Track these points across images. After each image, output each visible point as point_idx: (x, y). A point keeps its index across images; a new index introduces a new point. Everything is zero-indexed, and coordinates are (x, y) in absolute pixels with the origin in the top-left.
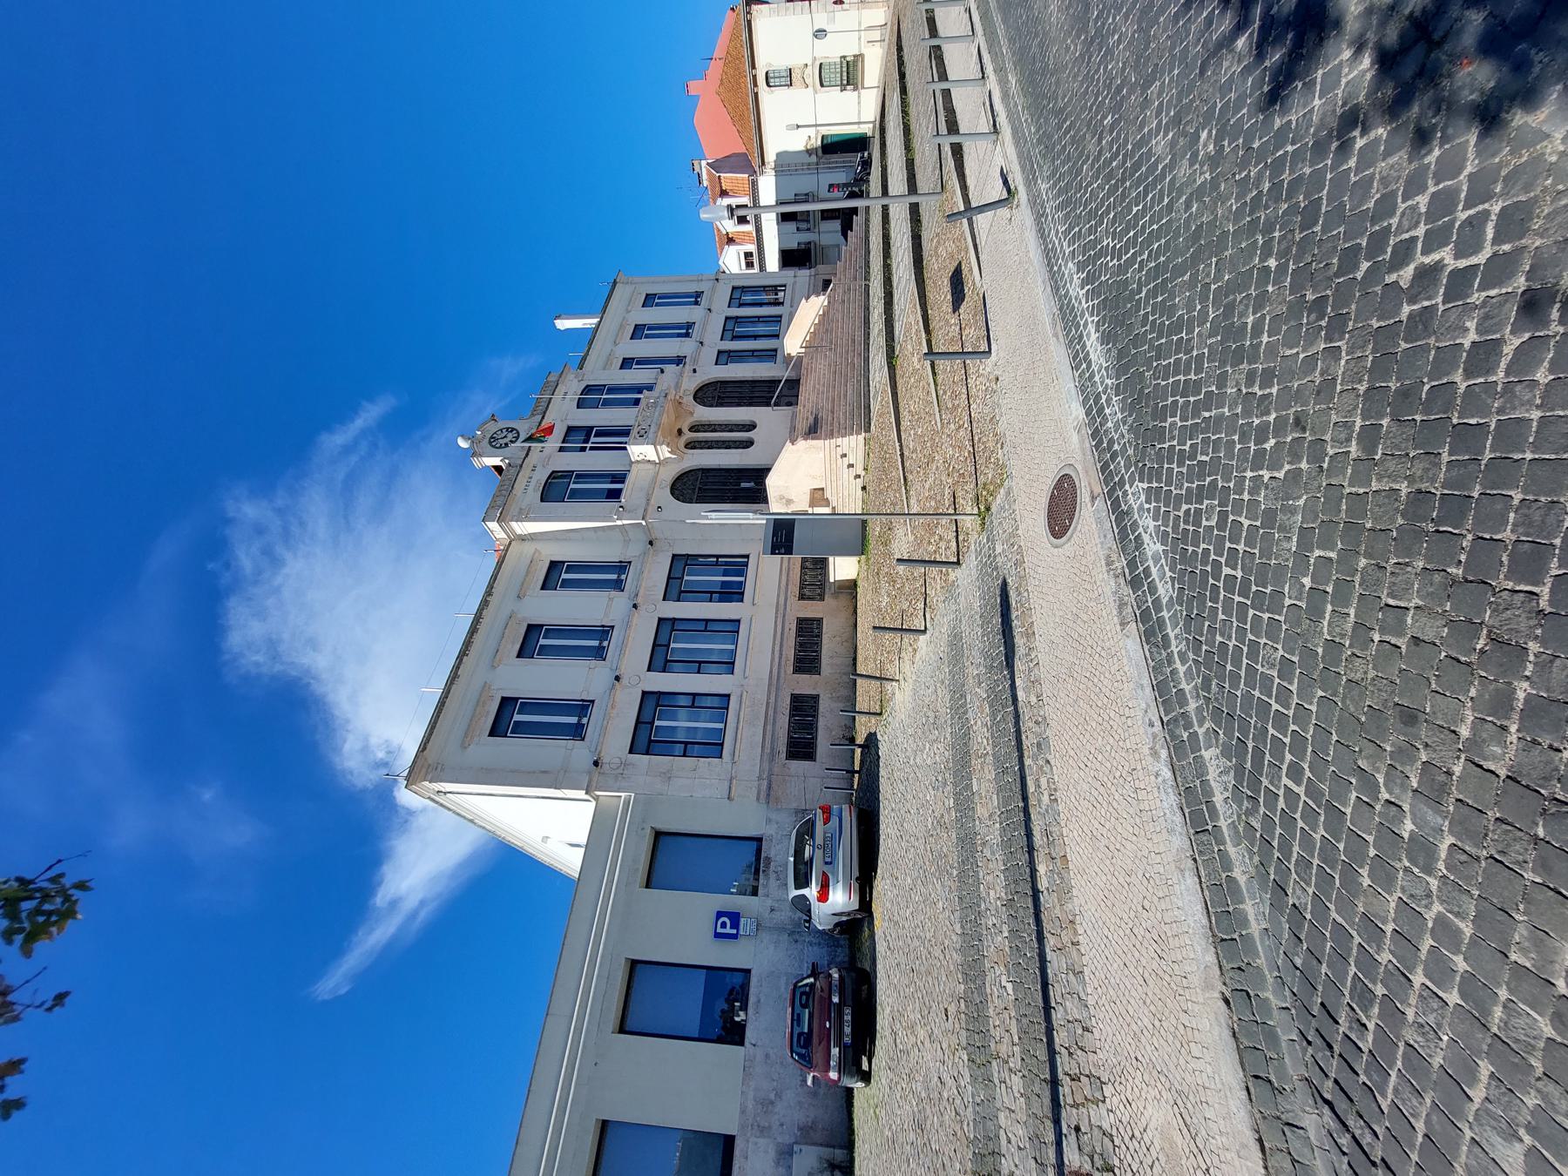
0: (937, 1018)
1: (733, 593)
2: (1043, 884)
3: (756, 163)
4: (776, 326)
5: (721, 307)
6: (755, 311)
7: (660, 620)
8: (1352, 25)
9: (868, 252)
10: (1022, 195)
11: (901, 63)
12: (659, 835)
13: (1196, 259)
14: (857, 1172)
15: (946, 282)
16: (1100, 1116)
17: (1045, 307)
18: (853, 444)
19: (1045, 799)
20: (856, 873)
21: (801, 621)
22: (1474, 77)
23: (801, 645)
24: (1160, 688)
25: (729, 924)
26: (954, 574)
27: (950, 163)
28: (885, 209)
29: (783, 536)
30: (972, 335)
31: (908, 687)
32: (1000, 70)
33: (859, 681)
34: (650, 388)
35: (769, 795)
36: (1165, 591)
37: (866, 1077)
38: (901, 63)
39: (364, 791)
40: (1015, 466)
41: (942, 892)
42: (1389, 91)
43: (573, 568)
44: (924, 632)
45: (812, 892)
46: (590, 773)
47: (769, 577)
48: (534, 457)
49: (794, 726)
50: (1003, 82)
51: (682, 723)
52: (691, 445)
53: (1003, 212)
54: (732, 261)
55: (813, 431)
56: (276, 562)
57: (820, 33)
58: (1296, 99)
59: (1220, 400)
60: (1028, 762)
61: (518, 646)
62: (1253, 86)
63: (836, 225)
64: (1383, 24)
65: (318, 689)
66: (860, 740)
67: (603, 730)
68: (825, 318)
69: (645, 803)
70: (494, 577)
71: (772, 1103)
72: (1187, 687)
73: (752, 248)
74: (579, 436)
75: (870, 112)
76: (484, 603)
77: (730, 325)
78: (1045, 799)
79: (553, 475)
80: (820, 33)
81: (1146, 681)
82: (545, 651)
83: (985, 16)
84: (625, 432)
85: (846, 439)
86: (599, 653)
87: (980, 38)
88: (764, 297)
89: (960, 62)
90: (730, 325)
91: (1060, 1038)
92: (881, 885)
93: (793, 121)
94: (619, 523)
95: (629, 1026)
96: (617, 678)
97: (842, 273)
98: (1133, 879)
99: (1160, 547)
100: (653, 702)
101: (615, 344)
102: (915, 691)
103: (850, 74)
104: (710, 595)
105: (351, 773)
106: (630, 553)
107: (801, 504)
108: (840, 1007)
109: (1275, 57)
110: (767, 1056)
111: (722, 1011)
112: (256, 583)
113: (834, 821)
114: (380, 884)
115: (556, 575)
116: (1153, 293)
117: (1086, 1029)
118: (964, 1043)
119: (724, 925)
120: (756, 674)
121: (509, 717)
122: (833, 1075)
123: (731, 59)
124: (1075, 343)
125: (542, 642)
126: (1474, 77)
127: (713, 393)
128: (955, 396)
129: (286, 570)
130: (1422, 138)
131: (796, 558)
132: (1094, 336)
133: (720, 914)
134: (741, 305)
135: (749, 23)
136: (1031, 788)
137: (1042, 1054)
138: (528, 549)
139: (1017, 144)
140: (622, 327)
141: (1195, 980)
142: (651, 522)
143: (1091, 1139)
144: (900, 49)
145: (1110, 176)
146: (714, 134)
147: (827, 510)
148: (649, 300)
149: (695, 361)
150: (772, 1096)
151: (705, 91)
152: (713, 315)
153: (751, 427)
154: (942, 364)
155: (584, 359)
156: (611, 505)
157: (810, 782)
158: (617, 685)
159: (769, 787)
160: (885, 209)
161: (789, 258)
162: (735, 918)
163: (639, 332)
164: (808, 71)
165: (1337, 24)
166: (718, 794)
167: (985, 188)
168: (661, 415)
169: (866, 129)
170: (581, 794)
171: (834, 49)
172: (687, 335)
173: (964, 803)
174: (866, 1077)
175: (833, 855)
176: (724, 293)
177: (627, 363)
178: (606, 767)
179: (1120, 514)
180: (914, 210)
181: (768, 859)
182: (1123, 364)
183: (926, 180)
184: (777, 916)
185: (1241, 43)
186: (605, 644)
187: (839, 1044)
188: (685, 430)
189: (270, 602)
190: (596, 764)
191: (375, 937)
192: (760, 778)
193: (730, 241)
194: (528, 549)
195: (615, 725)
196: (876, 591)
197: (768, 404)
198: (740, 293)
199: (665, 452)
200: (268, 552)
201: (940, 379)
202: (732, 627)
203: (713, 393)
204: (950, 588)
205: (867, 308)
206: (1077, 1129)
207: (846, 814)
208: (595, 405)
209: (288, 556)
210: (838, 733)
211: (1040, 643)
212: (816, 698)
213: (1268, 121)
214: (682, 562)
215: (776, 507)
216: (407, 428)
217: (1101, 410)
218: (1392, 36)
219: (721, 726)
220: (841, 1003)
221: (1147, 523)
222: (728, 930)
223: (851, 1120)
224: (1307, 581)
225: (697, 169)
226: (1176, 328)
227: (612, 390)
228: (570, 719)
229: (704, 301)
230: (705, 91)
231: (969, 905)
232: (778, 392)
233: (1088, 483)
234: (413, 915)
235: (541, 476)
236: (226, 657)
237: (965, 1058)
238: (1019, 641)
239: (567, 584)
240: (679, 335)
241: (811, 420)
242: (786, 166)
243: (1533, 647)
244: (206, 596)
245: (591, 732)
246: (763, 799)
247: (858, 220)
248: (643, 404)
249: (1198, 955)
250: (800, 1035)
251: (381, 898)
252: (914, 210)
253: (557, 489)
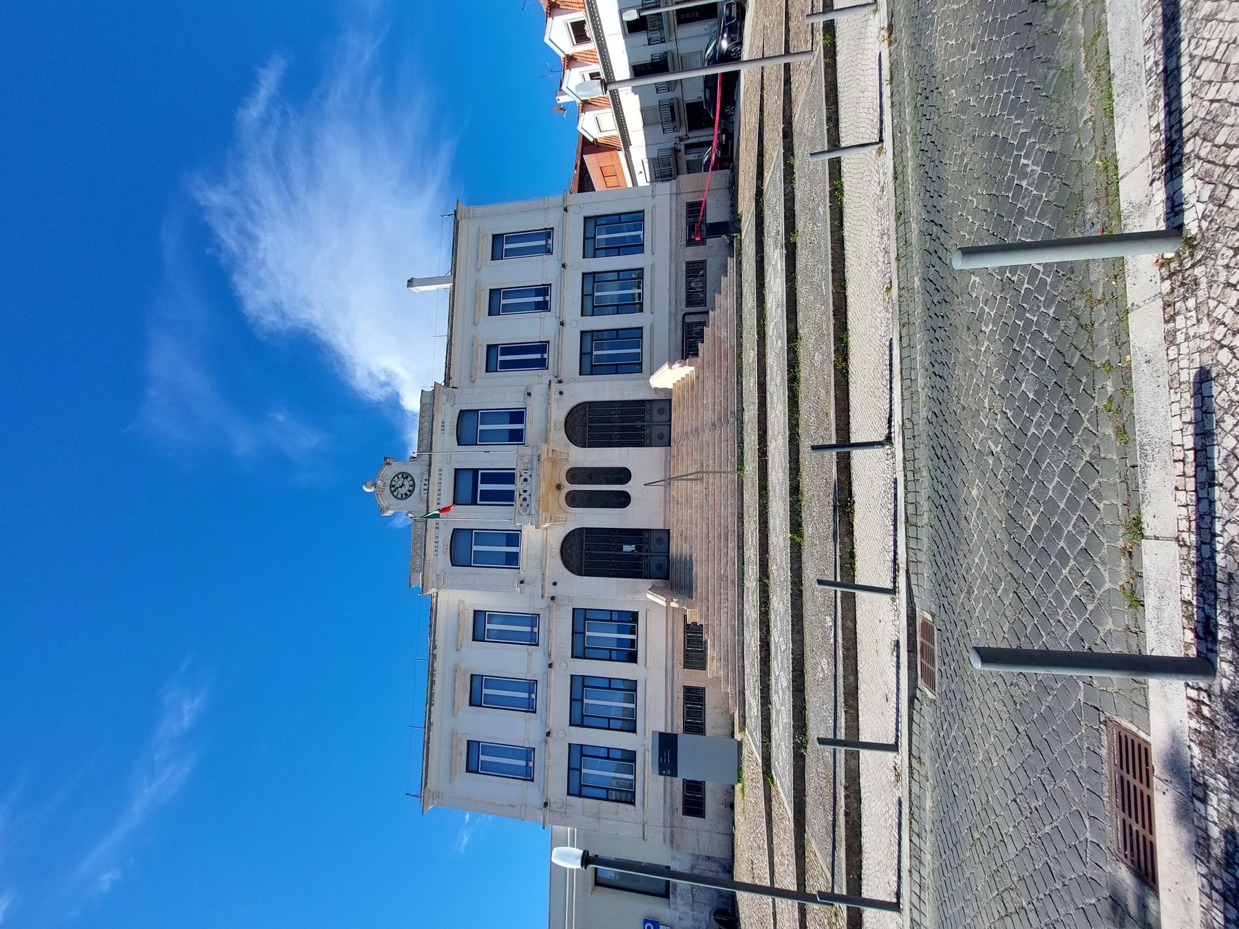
14: (743, 926)
39: (379, 403)
56: (253, 239)
65: (324, 337)
83: (898, 130)
87: (902, 757)
106: (538, 606)
112: (246, 259)
129: (261, 245)
152: (567, 328)
153: (622, 475)
156: (509, 573)
159: (672, 833)
178: (553, 807)
189: (262, 273)
195: (567, 353)
200: (242, 231)
202: (630, 688)
209: (258, 232)
210: (721, 795)
216: (303, 88)
219: (639, 350)
223: (733, 844)
228: (522, 765)
236: (250, 320)
244: (217, 281)
245: (553, 305)
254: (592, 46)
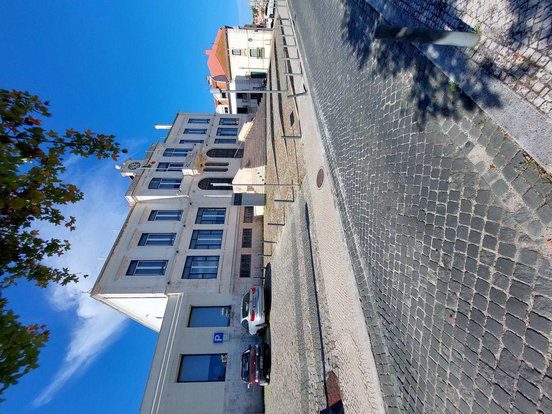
0: (290, 347)
1: (221, 221)
2: (318, 289)
3: (229, 78)
4: (235, 132)
5: (217, 125)
6: (229, 127)
7: (194, 230)
8: (373, 52)
9: (266, 109)
10: (309, 92)
11: (275, 50)
12: (193, 308)
13: (347, 107)
15: (289, 117)
16: (335, 352)
17: (315, 123)
18: (261, 169)
19: (318, 264)
20: (264, 310)
21: (244, 230)
22: (392, 65)
23: (245, 238)
24: (344, 222)
25: (219, 338)
26: (293, 205)
27: (290, 82)
28: (271, 94)
29: (238, 199)
30: (296, 133)
31: (279, 244)
32: (303, 56)
33: (265, 244)
34: (191, 150)
35: (234, 290)
36: (344, 196)
37: (268, 381)
38: (275, 50)
39: (64, 312)
40: (308, 169)
41: (290, 305)
42: (380, 67)
43: (161, 212)
44: (284, 225)
45: (248, 318)
46: (166, 287)
47: (234, 214)
48: (146, 173)
49: (242, 266)
50: (304, 60)
51: (200, 267)
52: (205, 170)
53: (304, 96)
54: (220, 110)
55: (248, 165)
57: (250, 40)
58: (364, 68)
59: (351, 143)
60: (313, 255)
61: (138, 242)
62: (356, 64)
63: (256, 101)
64: (378, 52)
66: (265, 266)
67: (179, 241)
68: (252, 129)
69: (188, 296)
70: (129, 216)
71: (235, 400)
72: (349, 220)
73: (227, 106)
74: (163, 166)
75: (267, 66)
76: (125, 226)
77: (222, 121)
78: (318, 264)
79: (154, 179)
80: (250, 40)
81: (341, 221)
82: (149, 243)
83: (299, 41)
84: (181, 165)
85: (259, 168)
86: (171, 243)
87: (298, 47)
88: (231, 122)
89: (292, 52)
90: (220, 131)
91: (324, 334)
92: (272, 313)
93: (242, 66)
94: (179, 196)
95: (181, 380)
96: (177, 252)
97: (258, 116)
98: (340, 278)
99: (343, 184)
100: (191, 260)
101: (178, 135)
102: (282, 245)
103: (260, 54)
104: (212, 221)
105: (57, 304)
107: (244, 190)
108: (259, 357)
109: (361, 57)
110: (233, 384)
111: (216, 369)
113: (256, 293)
114: (69, 351)
115: (154, 215)
116: (339, 117)
117: (330, 328)
118: (297, 350)
119: (217, 338)
120: (229, 249)
121: (133, 268)
122: (257, 381)
123: (220, 44)
124: (322, 132)
125: (137, 268)
126: (392, 65)
127: (213, 153)
128: (292, 151)
130: (385, 77)
131: (243, 206)
132: (327, 130)
133: (216, 334)
134: (223, 124)
135: (227, 34)
136: (314, 263)
137: (319, 342)
138: (143, 206)
139: (307, 77)
140: (180, 129)
141: (354, 299)
142: (190, 194)
143: (333, 360)
144: (275, 47)
145: (329, 86)
146: (214, 67)
147: (253, 192)
148: (191, 121)
149: (207, 142)
150: (235, 398)
151: (211, 54)
152: (213, 127)
154: (288, 141)
155: (166, 139)
156: (177, 190)
157: (247, 284)
158: (177, 255)
159: (234, 287)
160: (271, 94)
161: (240, 110)
162: (221, 335)
163: (186, 131)
164: (246, 51)
165: (371, 52)
166: (214, 292)
167: (299, 89)
168: (195, 160)
169: (266, 71)
170: (163, 295)
171: (255, 45)
172: (204, 133)
173: (296, 275)
174: (268, 381)
175: (256, 304)
176: (217, 120)
177: (182, 142)
178: (172, 284)
179: (334, 177)
180: (280, 95)
181: (233, 313)
182: (333, 136)
183: (283, 87)
184: (237, 333)
185: (354, 54)
186: (173, 239)
187: (259, 369)
188: (204, 165)
190: (169, 283)
191: (66, 374)
192: (230, 285)
193: (220, 103)
194: (143, 206)
196: (269, 216)
197: (233, 157)
198: (223, 120)
199: (196, 172)
201: (287, 146)
202: (220, 233)
203: (213, 153)
204: (291, 209)
205: (266, 126)
206: (329, 359)
207: (260, 290)
208: (170, 155)
211: (315, 219)
212: (250, 256)
213: (360, 73)
214: (202, 211)
215: (236, 191)
217: (329, 150)
218: (380, 56)
220: (259, 357)
221: (340, 178)
222: (219, 340)
223: (263, 401)
224: (370, 183)
225: (208, 79)
226: (344, 125)
227: (176, 150)
228: (159, 267)
229: (210, 122)
230: (211, 54)
231: (298, 306)
232: (236, 154)
233: (326, 170)
234: (84, 363)
235: (149, 180)
237: (298, 355)
238: (310, 220)
239: (158, 219)
240: (201, 133)
241: (248, 162)
242: (239, 80)
243: (406, 185)
245: (182, 218)
246: (231, 292)
247: (263, 99)
248: (188, 155)
249: (354, 290)
250: (245, 372)
251: (69, 357)
252: (280, 95)
253: (155, 185)
254: (226, 100)
